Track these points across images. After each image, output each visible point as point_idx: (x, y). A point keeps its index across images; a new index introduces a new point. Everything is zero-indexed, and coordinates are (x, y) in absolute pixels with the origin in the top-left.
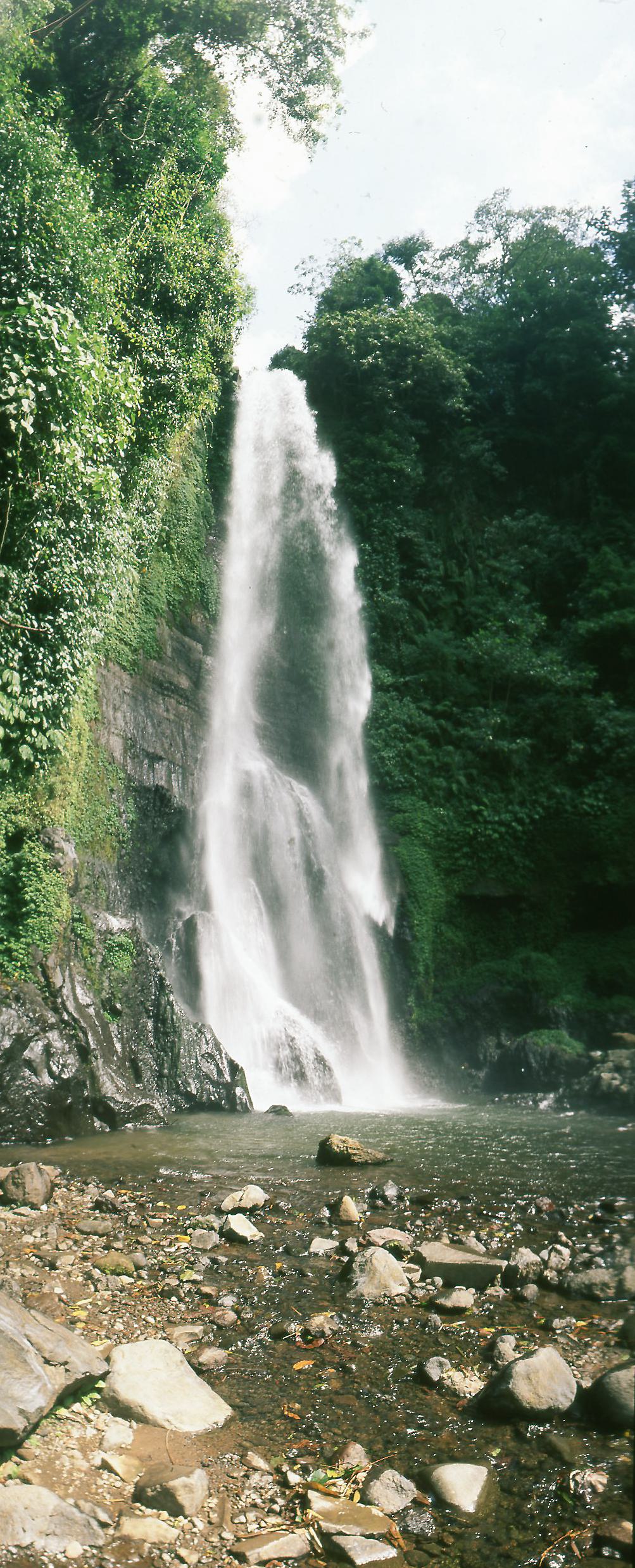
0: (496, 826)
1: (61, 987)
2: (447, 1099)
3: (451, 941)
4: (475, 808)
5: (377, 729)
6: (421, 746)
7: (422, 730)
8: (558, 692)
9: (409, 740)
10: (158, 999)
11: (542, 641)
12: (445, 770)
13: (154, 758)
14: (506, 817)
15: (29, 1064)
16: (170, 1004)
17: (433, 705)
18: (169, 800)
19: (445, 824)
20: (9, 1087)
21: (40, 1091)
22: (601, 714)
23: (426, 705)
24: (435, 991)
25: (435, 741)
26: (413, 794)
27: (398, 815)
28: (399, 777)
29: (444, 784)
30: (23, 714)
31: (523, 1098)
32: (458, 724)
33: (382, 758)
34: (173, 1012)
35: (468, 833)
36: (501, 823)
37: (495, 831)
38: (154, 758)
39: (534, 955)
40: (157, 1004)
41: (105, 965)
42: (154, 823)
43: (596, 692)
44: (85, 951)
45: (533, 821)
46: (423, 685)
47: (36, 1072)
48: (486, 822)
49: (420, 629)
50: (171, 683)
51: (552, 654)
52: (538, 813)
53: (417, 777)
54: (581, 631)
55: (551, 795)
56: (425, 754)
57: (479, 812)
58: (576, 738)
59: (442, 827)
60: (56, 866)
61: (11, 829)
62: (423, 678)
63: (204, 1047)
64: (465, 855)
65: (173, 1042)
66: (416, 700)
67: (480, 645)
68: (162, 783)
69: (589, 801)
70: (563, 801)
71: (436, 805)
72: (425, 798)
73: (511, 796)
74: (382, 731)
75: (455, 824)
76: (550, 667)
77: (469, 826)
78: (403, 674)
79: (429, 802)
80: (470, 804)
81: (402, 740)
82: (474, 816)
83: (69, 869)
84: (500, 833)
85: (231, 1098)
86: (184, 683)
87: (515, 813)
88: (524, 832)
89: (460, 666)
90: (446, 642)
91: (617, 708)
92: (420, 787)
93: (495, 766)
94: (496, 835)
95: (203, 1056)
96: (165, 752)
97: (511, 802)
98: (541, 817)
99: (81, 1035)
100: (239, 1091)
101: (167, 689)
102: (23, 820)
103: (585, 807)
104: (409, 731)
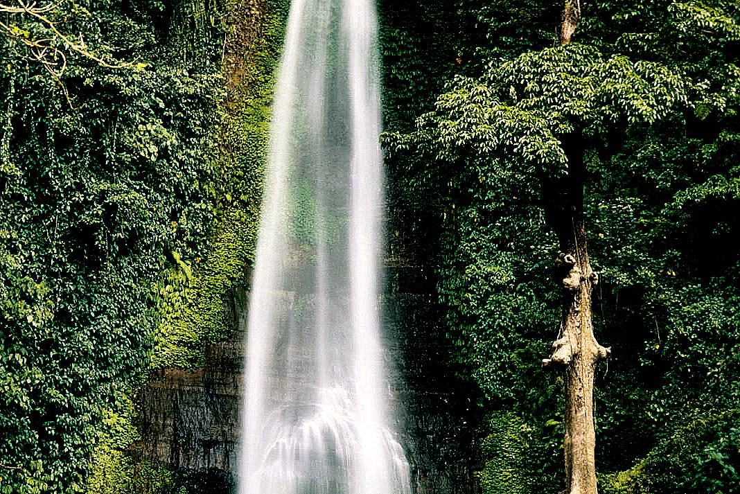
26: (511, 409)
64: (547, 470)
104: (524, 336)
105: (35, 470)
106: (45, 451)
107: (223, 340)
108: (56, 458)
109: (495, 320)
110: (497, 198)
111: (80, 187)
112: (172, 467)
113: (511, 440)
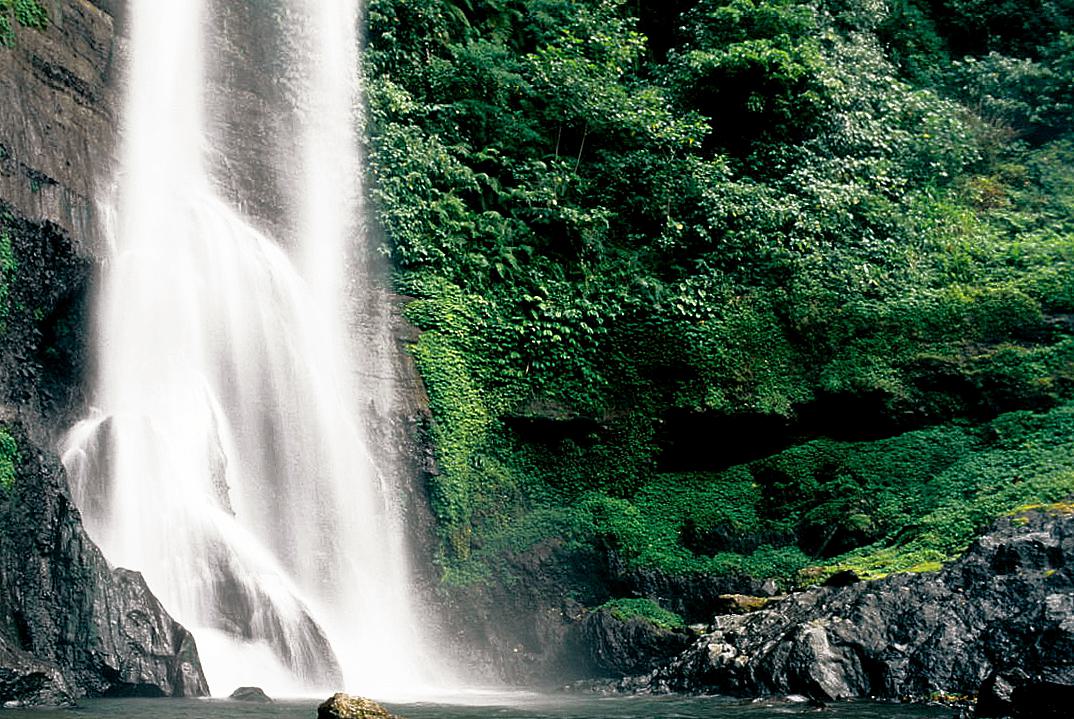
2: (513, 677)
4: (529, 298)
5: (389, 176)
6: (454, 207)
7: (456, 184)
8: (654, 150)
9: (435, 197)
11: (639, 72)
12: (487, 241)
13: (42, 180)
14: (574, 313)
17: (472, 152)
18: (68, 246)
22: (710, 185)
23: (463, 149)
24: (474, 547)
25: (473, 201)
26: (441, 274)
28: (419, 246)
29: (485, 263)
31: (603, 684)
32: (508, 181)
33: (396, 219)
35: (518, 333)
36: (564, 321)
37: (555, 331)
38: (42, 180)
39: (610, 502)
42: (43, 276)
43: (706, 154)
45: (608, 322)
46: (459, 119)
48: (542, 318)
49: (458, 36)
50: (64, 70)
51: (651, 93)
52: (615, 311)
53: (445, 250)
54: (694, 64)
55: (635, 289)
56: (459, 219)
57: (534, 305)
58: (674, 215)
59: (480, 321)
62: (460, 108)
63: (132, 603)
64: (513, 363)
66: (450, 141)
67: (547, 67)
68: (55, 219)
69: (686, 298)
71: (473, 291)
72: (458, 280)
74: (396, 179)
76: (648, 110)
77: (519, 322)
78: (430, 100)
79: (463, 286)
80: (522, 293)
81: (425, 197)
82: (526, 308)
84: (563, 335)
85: (177, 681)
86: (85, 72)
87: (584, 310)
88: (595, 336)
89: (514, 99)
90: (497, 60)
91: (733, 179)
92: (450, 265)
93: (557, 243)
95: (129, 616)
96: (59, 174)
97: (579, 294)
98: (619, 317)
100: (186, 667)
113: (455, 312)
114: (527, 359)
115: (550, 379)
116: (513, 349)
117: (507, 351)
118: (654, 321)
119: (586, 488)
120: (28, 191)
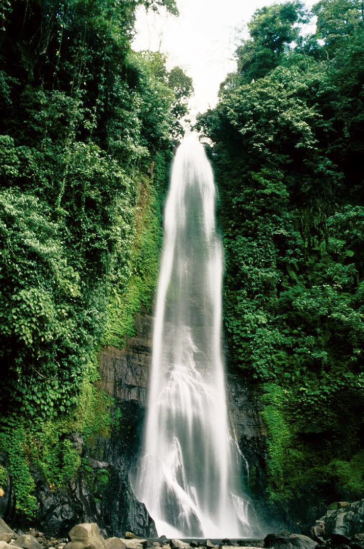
0: (312, 398)
1: (75, 490)
3: (295, 457)
10: (122, 493)
14: (318, 392)
15: (55, 514)
16: (126, 494)
19: (288, 398)
20: (48, 521)
21: (59, 522)
24: (286, 484)
26: (274, 383)
27: (265, 395)
30: (60, 396)
34: (127, 498)
36: (315, 396)
37: (312, 400)
40: (121, 495)
41: (96, 480)
44: (88, 477)
45: (332, 393)
47: (57, 516)
48: (307, 396)
50: (142, 346)
53: (276, 374)
55: (343, 379)
60: (74, 447)
61: (61, 434)
62: (285, 316)
64: (299, 413)
65: (126, 510)
70: (349, 381)
72: (280, 385)
73: (322, 381)
75: (293, 398)
77: (300, 398)
83: (80, 448)
93: (315, 366)
94: (313, 402)
97: (321, 384)
99: (80, 506)
101: (141, 350)
102: (65, 431)
103: (359, 384)
104: (276, 349)
105: (54, 386)
106: (60, 375)
107: (133, 336)
108: (66, 380)
109: (263, 339)
110: (257, 286)
111: (94, 231)
112: (115, 396)
113: (278, 397)
114: (304, 411)
115: (314, 418)
116: (298, 408)
117: (296, 410)
118: (351, 390)
119: (333, 458)
120: (127, 392)
